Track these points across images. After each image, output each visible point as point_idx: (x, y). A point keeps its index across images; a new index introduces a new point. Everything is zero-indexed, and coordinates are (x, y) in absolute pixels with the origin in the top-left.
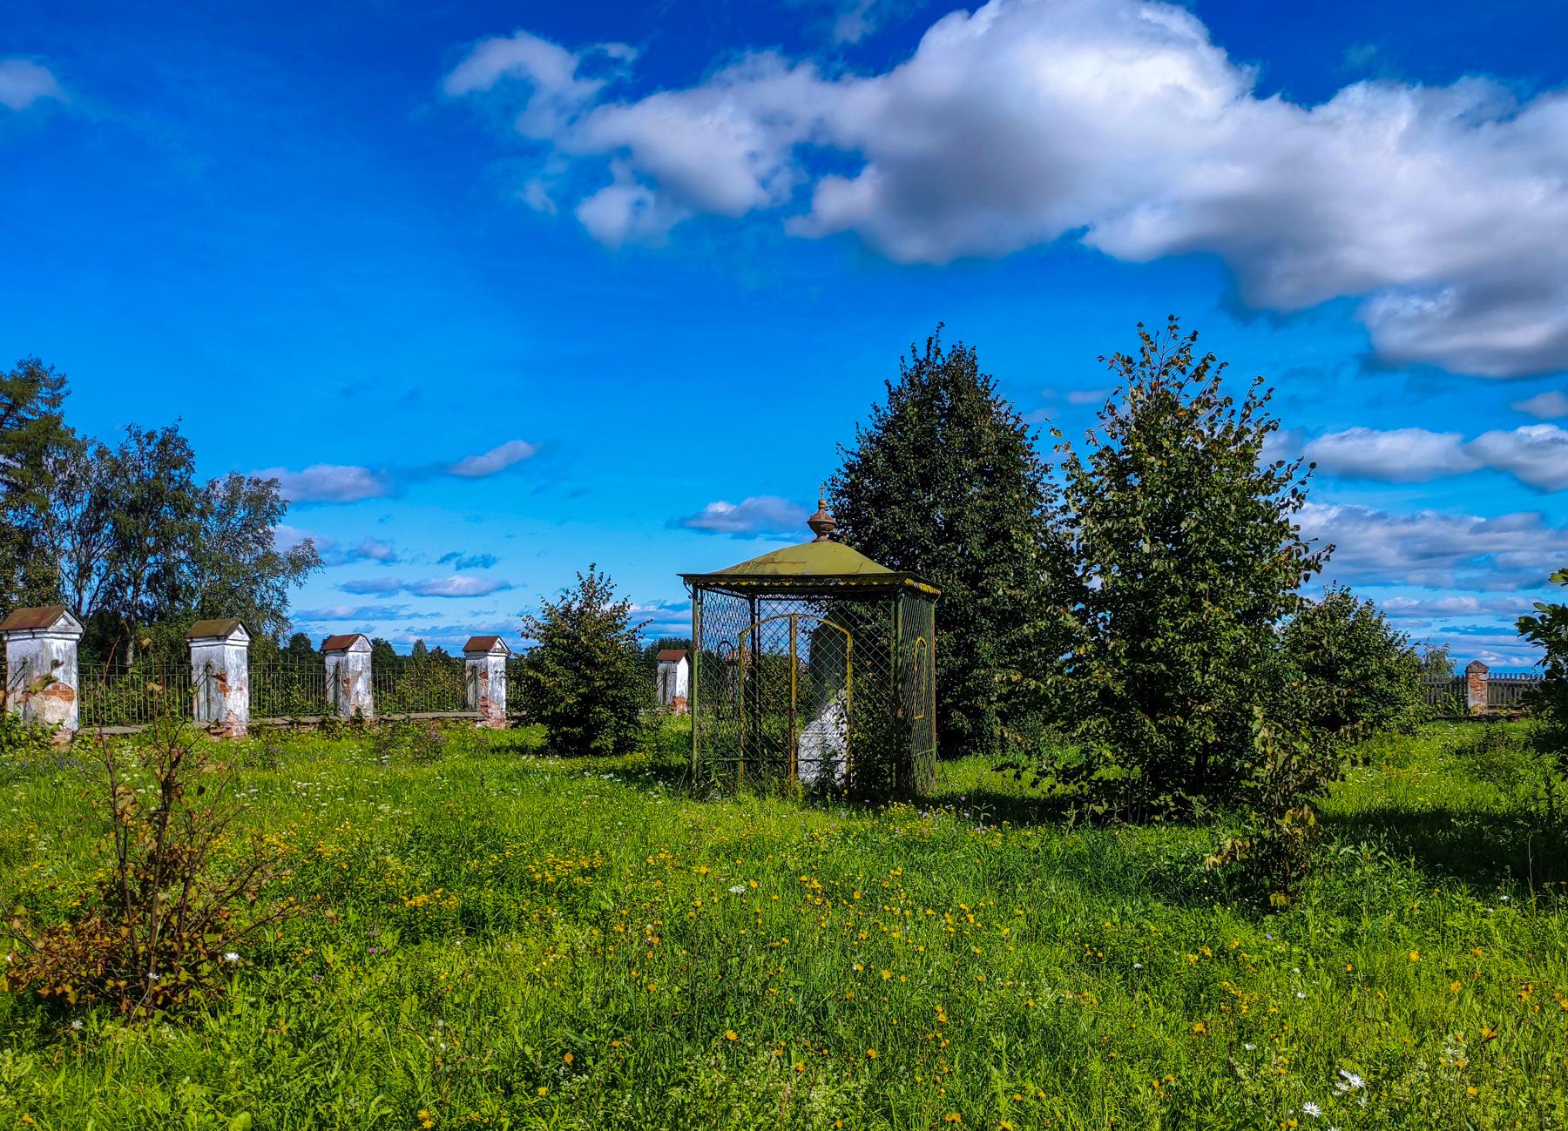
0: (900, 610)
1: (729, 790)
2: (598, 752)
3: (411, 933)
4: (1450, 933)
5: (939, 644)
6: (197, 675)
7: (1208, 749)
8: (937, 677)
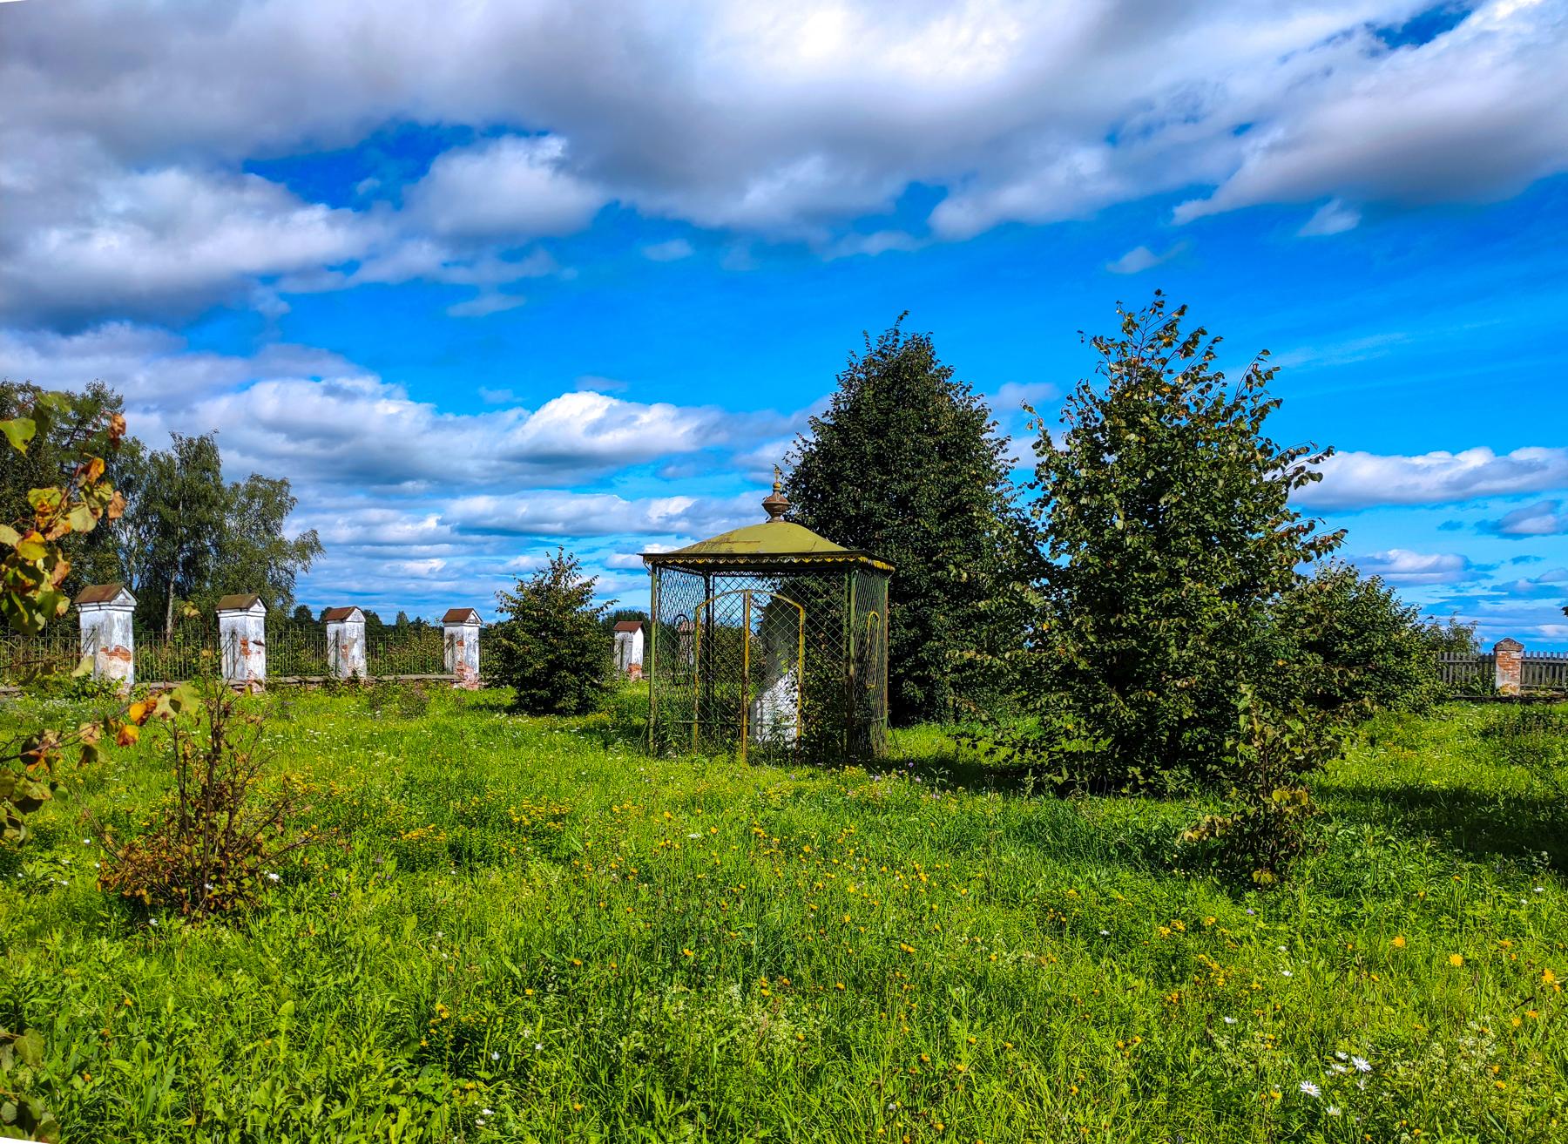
0: (853, 586)
1: (684, 748)
2: (562, 713)
3: (409, 862)
4: (1469, 922)
5: (892, 617)
6: (225, 640)
7: (1184, 725)
8: (890, 648)
